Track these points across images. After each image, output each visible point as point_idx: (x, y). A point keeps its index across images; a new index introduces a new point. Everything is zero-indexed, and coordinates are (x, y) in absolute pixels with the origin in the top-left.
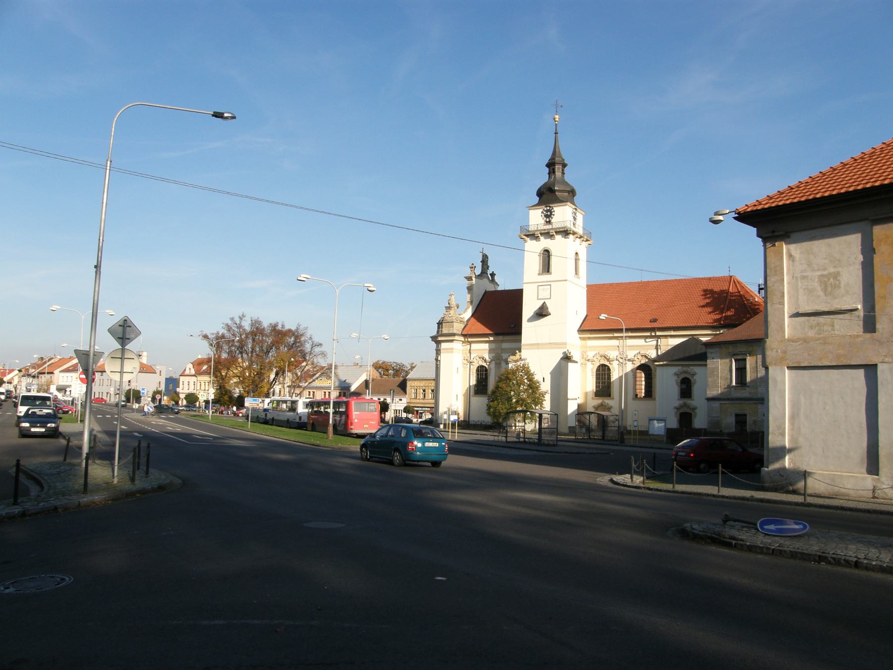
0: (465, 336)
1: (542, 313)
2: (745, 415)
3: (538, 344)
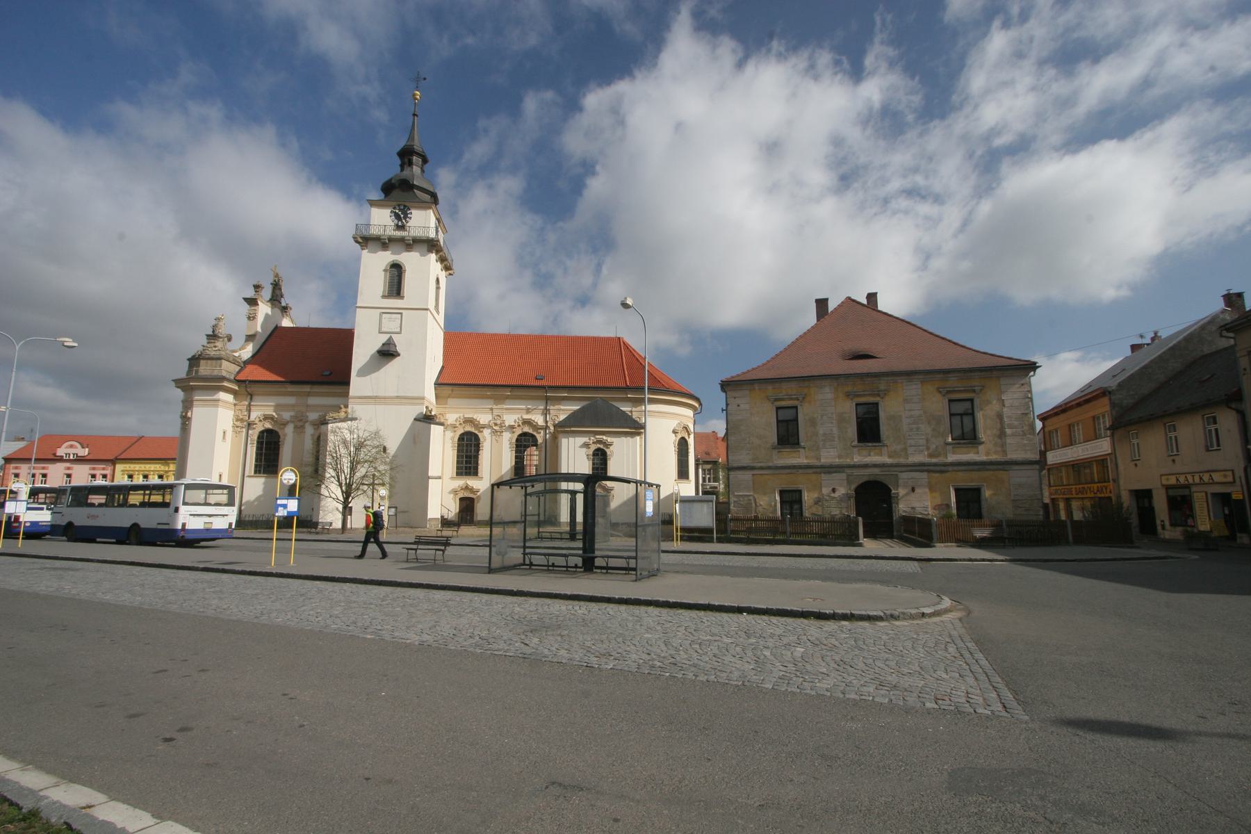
0: (238, 382)
1: (387, 353)
2: (800, 492)
3: (376, 397)
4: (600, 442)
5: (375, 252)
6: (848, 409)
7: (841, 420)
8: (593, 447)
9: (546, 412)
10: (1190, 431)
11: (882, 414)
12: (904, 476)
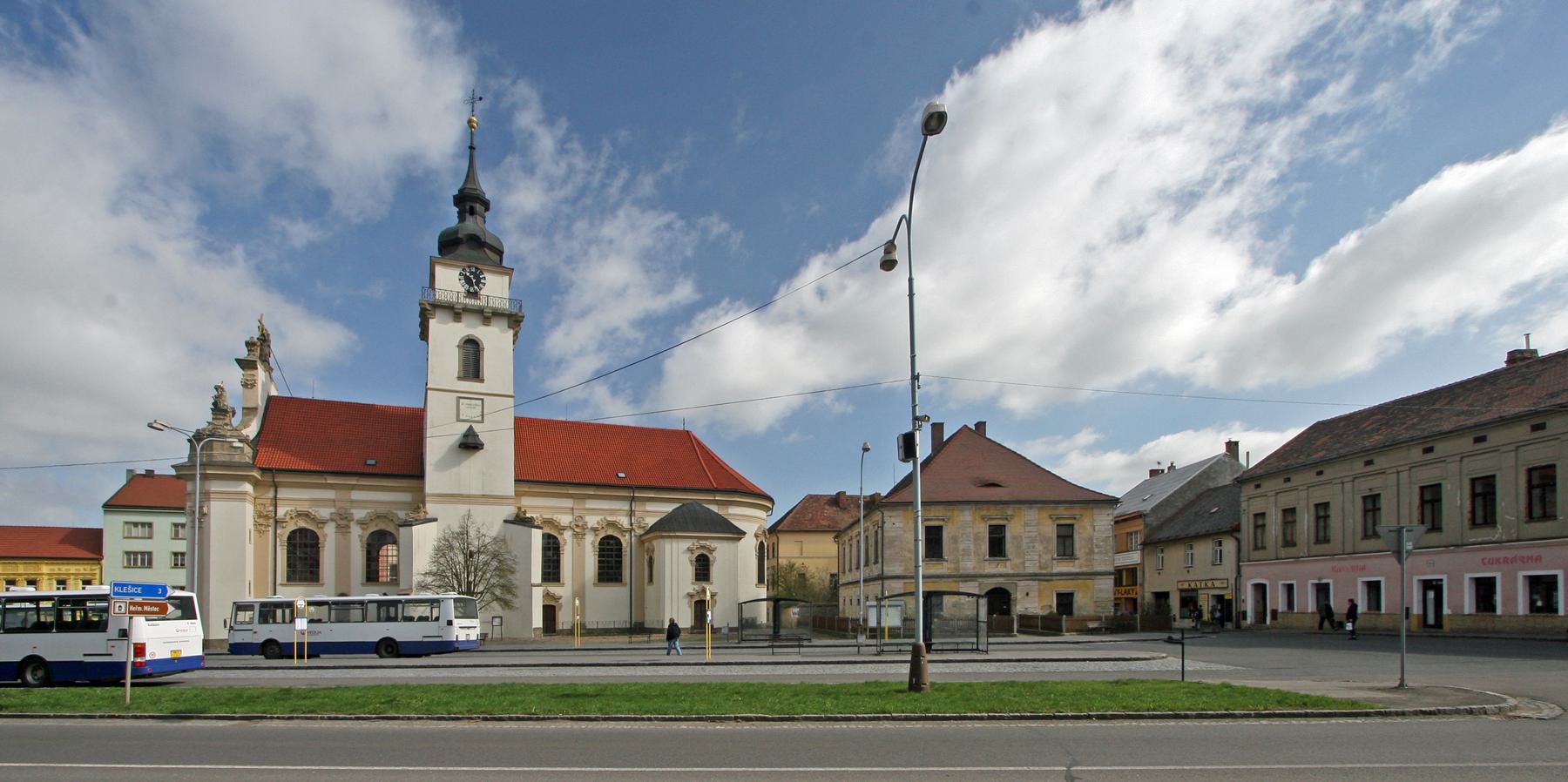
4: (703, 547)
5: (445, 323)
6: (983, 530)
7: (977, 538)
8: (697, 553)
9: (631, 513)
10: (1203, 550)
11: (1008, 535)
12: (1021, 583)
